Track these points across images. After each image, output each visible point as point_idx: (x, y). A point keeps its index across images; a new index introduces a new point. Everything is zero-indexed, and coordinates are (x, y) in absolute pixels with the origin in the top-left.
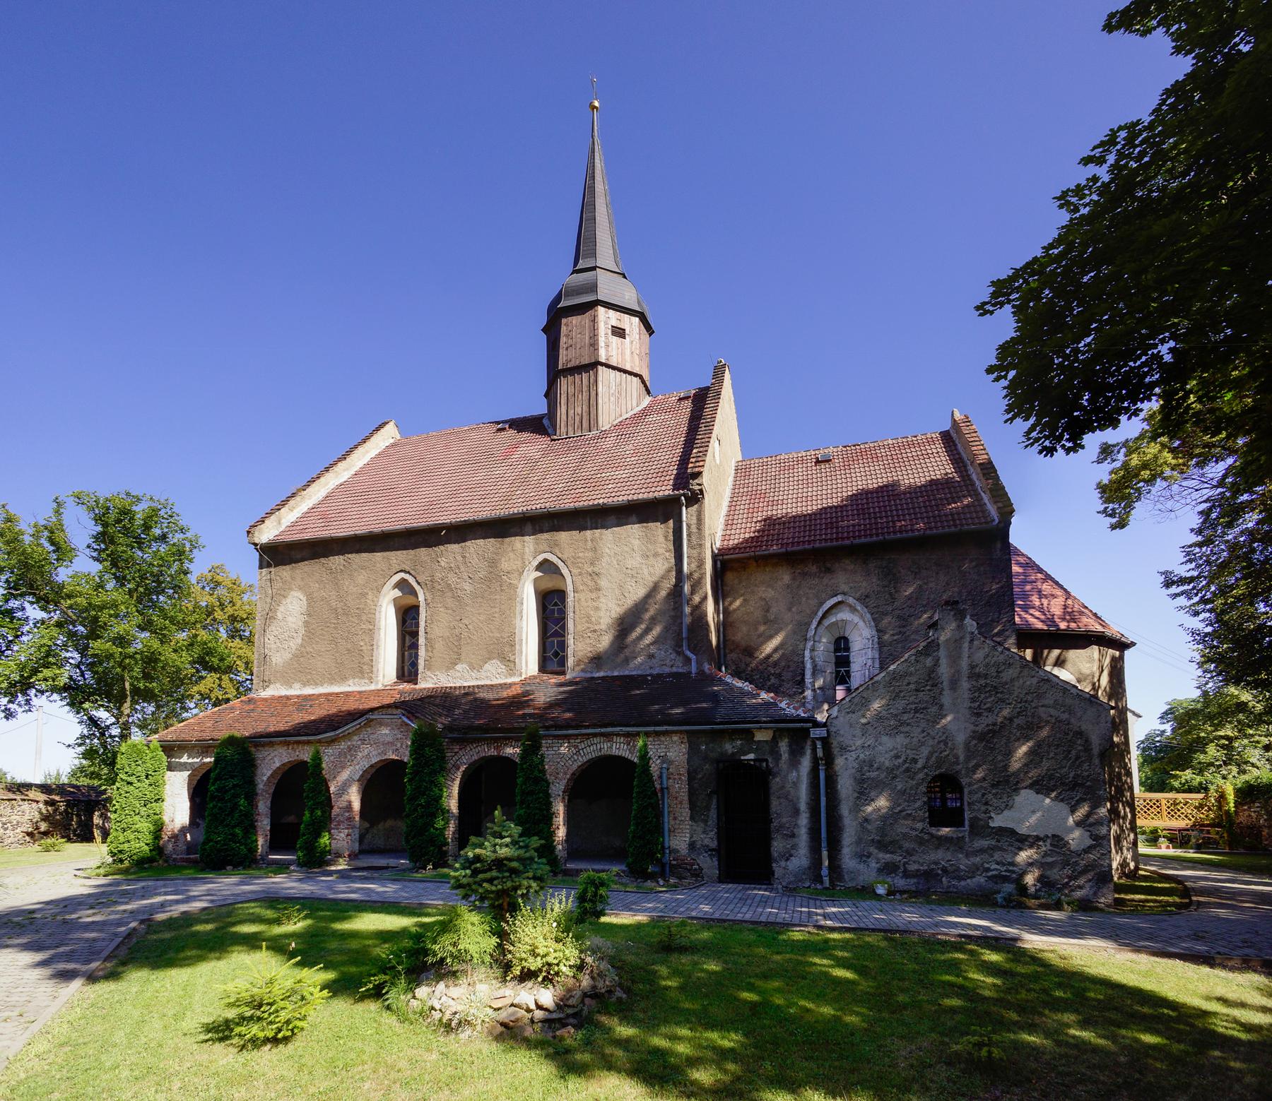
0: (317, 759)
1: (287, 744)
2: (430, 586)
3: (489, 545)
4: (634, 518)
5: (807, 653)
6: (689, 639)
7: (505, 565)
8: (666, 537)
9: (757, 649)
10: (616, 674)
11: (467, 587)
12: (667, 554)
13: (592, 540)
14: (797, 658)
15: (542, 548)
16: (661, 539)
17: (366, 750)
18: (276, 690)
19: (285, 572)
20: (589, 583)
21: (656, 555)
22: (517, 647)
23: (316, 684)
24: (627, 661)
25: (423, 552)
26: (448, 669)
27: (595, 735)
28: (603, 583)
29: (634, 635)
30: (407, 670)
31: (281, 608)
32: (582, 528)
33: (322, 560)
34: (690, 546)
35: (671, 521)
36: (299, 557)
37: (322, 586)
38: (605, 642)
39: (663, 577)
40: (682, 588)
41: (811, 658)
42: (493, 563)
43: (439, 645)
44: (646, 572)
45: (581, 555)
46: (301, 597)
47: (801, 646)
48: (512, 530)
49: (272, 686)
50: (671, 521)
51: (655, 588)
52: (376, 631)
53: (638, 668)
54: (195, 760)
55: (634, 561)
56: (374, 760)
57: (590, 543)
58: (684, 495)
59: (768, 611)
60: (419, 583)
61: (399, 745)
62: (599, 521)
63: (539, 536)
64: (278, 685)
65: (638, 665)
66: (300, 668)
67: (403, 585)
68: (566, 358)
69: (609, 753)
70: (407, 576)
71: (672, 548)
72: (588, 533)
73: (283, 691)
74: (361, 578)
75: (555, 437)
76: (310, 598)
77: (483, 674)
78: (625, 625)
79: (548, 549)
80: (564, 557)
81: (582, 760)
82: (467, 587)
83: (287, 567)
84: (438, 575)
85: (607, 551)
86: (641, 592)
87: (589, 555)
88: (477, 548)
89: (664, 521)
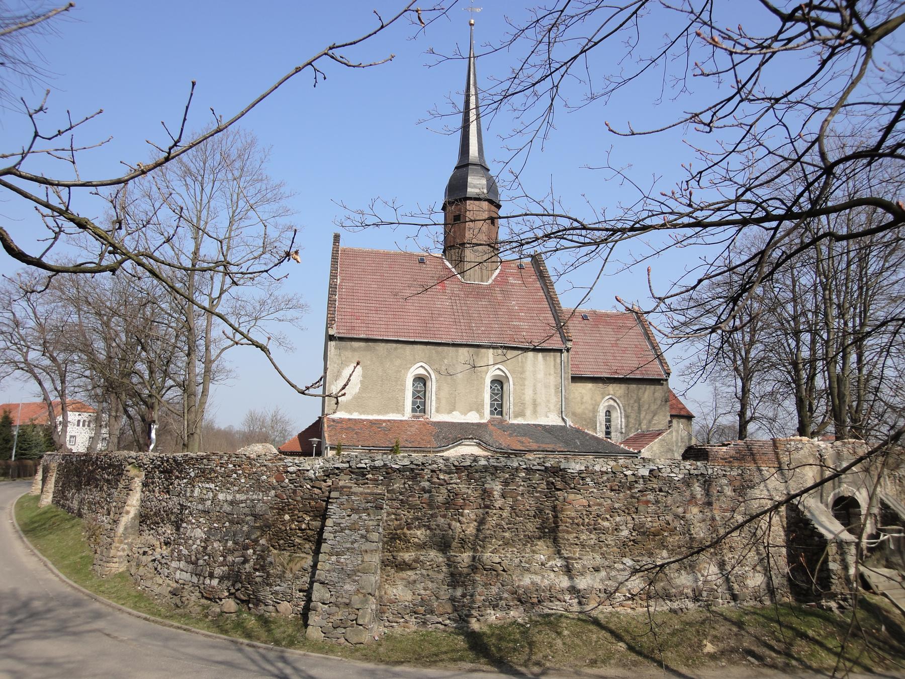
43: (443, 402)
57: (520, 364)
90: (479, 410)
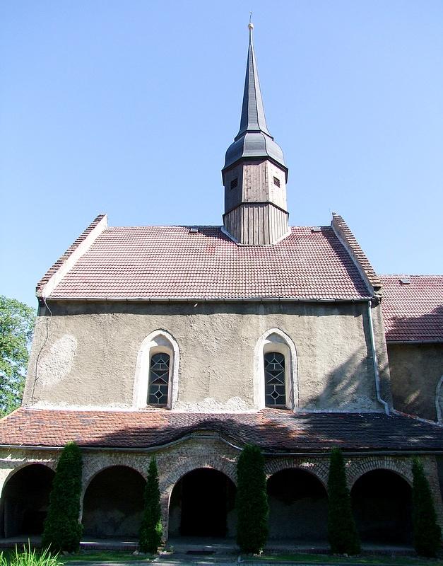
0: (153, 470)
1: (110, 452)
2: (185, 341)
3: (232, 319)
4: (336, 311)
5: (437, 403)
6: (380, 391)
7: (244, 333)
8: (359, 327)
9: (405, 398)
10: (330, 412)
11: (214, 345)
12: (361, 338)
13: (308, 323)
14: (431, 405)
15: (272, 325)
16: (356, 328)
17: (183, 460)
18: (42, 406)
19: (61, 320)
20: (308, 351)
21: (353, 338)
22: (254, 388)
23: (81, 403)
24: (337, 403)
25: (179, 318)
26: (198, 400)
27: (371, 456)
28: (317, 351)
29: (340, 387)
30: (158, 395)
31: (55, 345)
32: (301, 314)
33: (94, 315)
34: (376, 335)
35: (361, 316)
36: (74, 311)
37: (92, 333)
38: (320, 389)
39: (358, 351)
40: (373, 359)
41: (440, 406)
42: (235, 331)
44: (347, 347)
45: (301, 332)
46: (73, 339)
47: (433, 398)
48: (249, 309)
49: (40, 402)
50: (361, 316)
51: (353, 357)
52: (137, 369)
53: (345, 407)
54: (19, 460)
55: (339, 340)
56: (191, 469)
58: (371, 300)
59: (410, 376)
60: (174, 339)
61: (213, 458)
62: (312, 309)
63: (269, 316)
64: (46, 402)
65: (345, 407)
66: (68, 388)
67: (159, 339)
68: (248, 194)
69: (382, 467)
70: (164, 333)
71: (363, 334)
72: (305, 317)
73: (50, 407)
74: (127, 331)
75: (240, 244)
76: (81, 340)
77: (227, 405)
78: (334, 380)
79: (276, 326)
80: (289, 333)
81: (362, 472)
82: (214, 345)
83: (63, 317)
84: (191, 335)
85: (319, 331)
86: (343, 360)
87: (307, 333)
88: (222, 320)
89: (357, 315)
90: (244, 392)
